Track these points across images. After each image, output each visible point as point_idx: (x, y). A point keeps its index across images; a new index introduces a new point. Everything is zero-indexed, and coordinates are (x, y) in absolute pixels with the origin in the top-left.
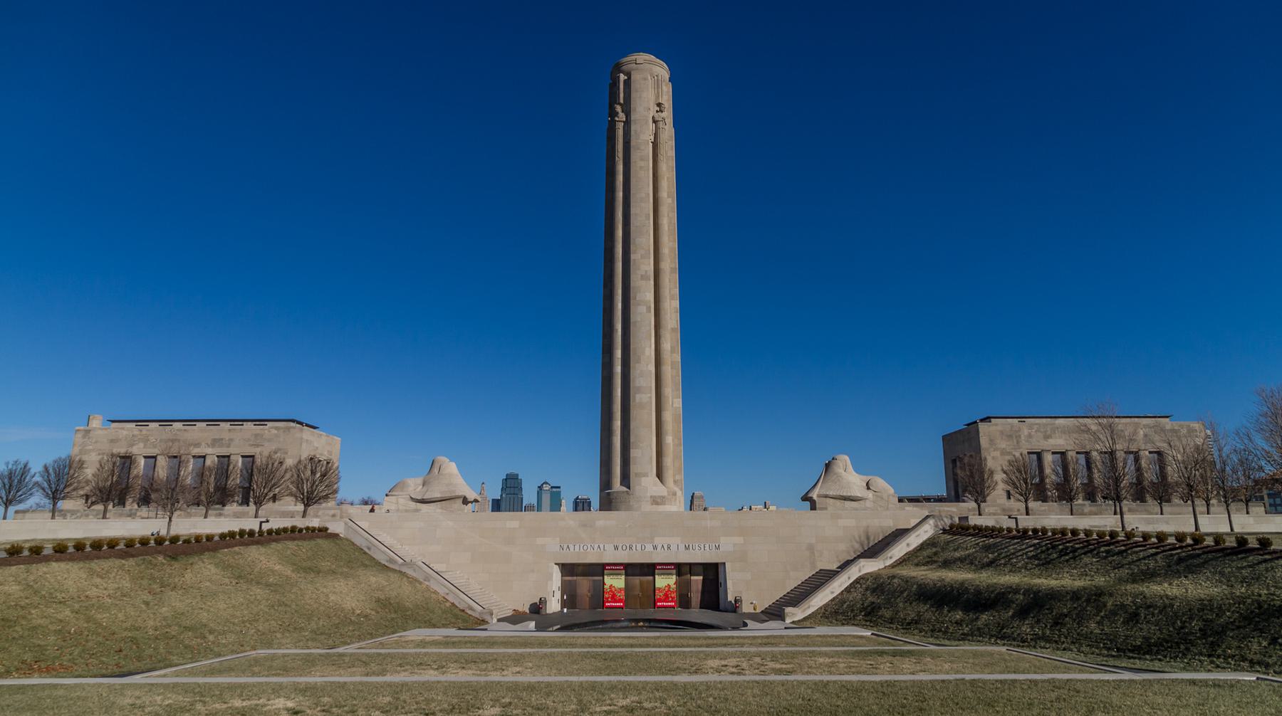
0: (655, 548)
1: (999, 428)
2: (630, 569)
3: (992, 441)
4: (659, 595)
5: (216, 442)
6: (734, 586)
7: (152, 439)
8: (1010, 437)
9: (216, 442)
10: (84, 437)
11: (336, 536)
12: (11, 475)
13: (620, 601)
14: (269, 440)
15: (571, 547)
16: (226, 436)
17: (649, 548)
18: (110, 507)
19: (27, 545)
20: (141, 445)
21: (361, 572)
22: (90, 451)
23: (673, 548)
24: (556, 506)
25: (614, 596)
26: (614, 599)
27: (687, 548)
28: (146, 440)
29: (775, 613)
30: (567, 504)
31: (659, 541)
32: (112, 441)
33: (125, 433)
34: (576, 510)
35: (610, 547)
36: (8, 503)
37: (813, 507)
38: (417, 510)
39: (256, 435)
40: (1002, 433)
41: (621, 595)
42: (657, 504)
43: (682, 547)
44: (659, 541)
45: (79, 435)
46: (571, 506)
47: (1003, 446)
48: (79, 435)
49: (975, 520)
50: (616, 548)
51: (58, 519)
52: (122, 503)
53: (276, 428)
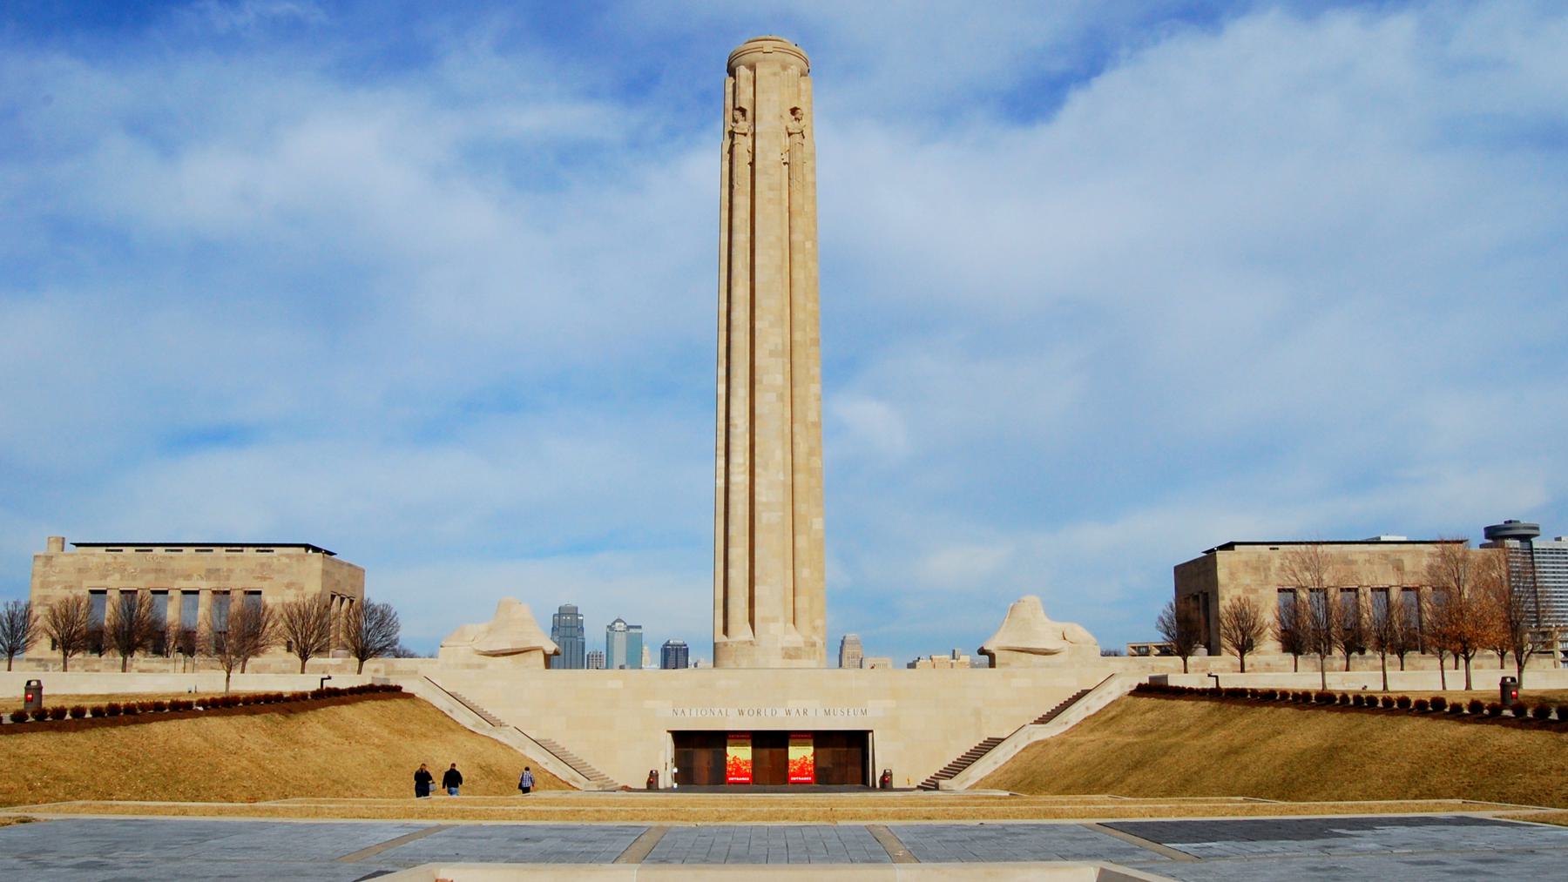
0: (788, 713)
1: (1244, 557)
2: (759, 739)
3: (1232, 575)
4: (792, 769)
5: (211, 573)
6: (883, 757)
7: (130, 569)
8: (1256, 569)
9: (211, 573)
10: (45, 565)
11: (410, 696)
12: (12, 617)
13: (746, 775)
14: (280, 572)
15: (687, 711)
16: (224, 565)
17: (781, 713)
18: (1388, 655)
19: (1487, 703)
20: (117, 576)
21: (451, 736)
22: (54, 583)
23: (811, 713)
24: (634, 661)
25: (739, 768)
26: (739, 772)
27: (827, 713)
28: (122, 570)
29: (931, 785)
30: (651, 658)
31: (792, 705)
32: (80, 570)
33: (95, 560)
34: (665, 666)
35: (733, 712)
36: (12, 652)
37: (992, 664)
38: (480, 666)
39: (262, 565)
40: (1246, 563)
41: (748, 769)
42: (790, 657)
43: (821, 712)
44: (792, 705)
45: (39, 563)
46: (658, 655)
47: (1248, 581)
48: (39, 563)
49: (1176, 680)
50: (741, 713)
51: (849, 673)
52: (1362, 651)
53: (288, 556)
